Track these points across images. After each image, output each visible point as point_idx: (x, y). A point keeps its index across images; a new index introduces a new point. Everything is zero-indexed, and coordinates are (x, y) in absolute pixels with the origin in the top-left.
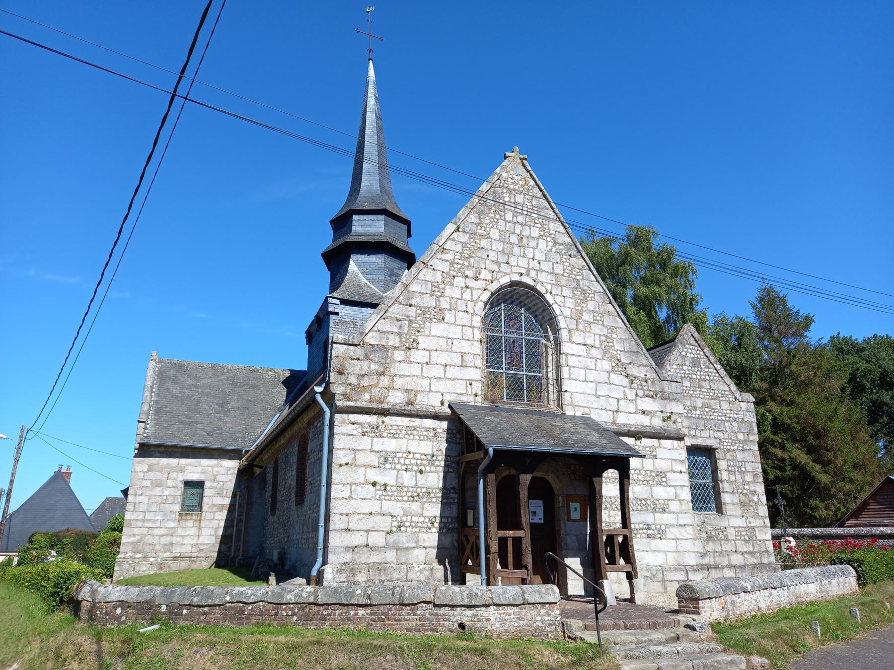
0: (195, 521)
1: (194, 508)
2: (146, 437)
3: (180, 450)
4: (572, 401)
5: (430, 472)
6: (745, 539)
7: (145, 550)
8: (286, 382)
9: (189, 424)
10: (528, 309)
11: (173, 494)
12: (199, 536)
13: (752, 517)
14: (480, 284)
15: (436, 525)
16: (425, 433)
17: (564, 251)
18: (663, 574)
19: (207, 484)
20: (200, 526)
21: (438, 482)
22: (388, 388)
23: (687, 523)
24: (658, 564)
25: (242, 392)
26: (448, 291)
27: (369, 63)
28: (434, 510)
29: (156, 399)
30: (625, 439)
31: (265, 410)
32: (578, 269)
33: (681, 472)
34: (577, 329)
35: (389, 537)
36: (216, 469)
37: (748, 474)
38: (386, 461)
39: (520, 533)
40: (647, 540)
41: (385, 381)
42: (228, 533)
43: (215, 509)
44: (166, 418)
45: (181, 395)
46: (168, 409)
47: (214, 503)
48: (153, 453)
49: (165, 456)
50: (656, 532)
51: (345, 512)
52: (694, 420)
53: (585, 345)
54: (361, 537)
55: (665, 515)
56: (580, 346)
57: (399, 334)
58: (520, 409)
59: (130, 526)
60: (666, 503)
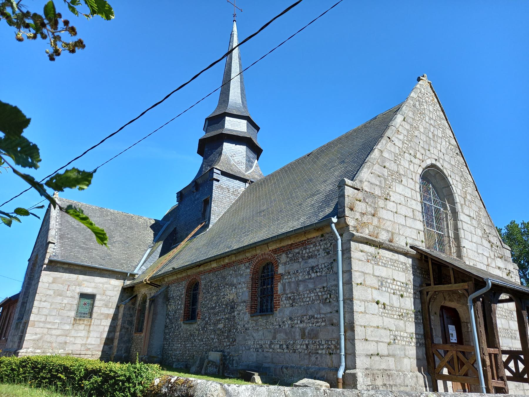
0: (86, 325)
1: (85, 315)
2: (54, 256)
3: (80, 268)
4: (467, 255)
7: (44, 347)
8: (152, 227)
9: (87, 249)
11: (70, 303)
12: (88, 337)
15: (414, 340)
16: (401, 266)
19: (98, 297)
20: (89, 330)
25: (122, 231)
27: (233, 25)
29: (59, 227)
31: (140, 245)
34: (465, 204)
35: (390, 347)
36: (106, 286)
38: (382, 284)
42: (110, 337)
43: (102, 317)
44: (69, 243)
45: (78, 227)
46: (69, 236)
47: (101, 312)
48: (59, 269)
49: (68, 272)
51: (363, 324)
53: (470, 216)
54: (374, 346)
59: (33, 326)
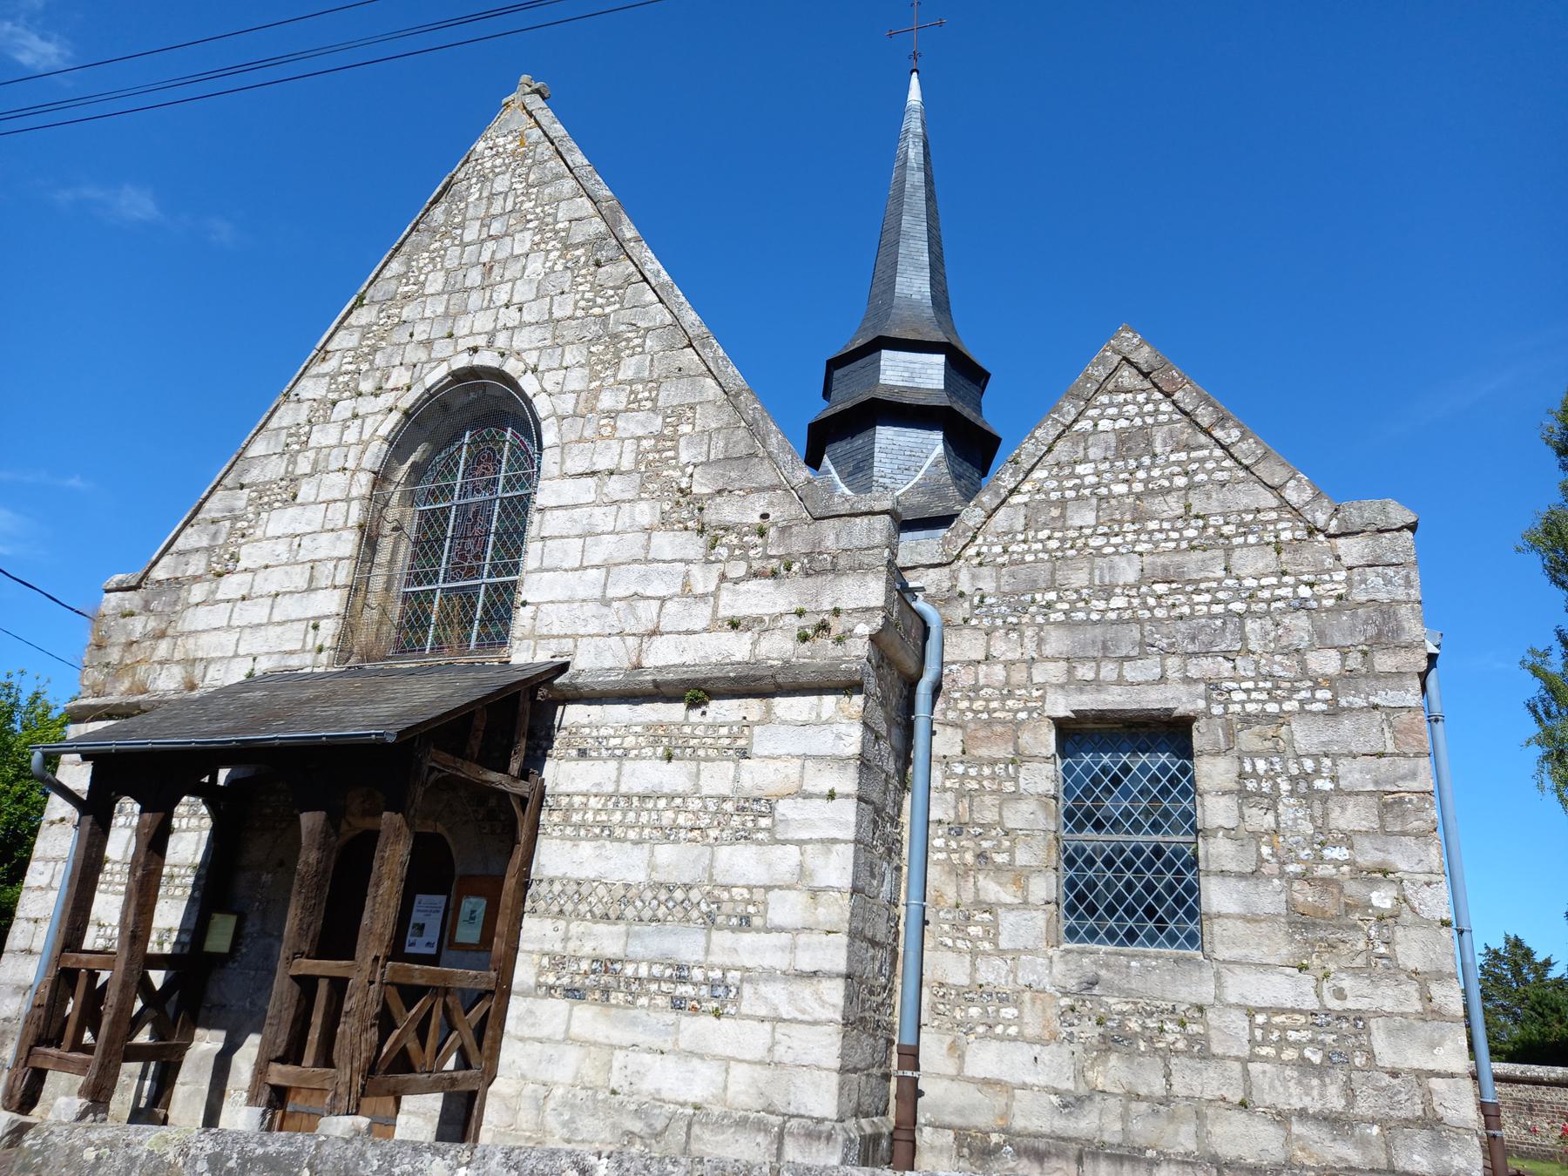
5: (188, 829)
6: (1303, 1058)
13: (1355, 972)
17: (583, 259)
18: (688, 1134)
21: (196, 853)
23: (826, 967)
24: (691, 1099)
32: (612, 288)
33: (832, 796)
37: (1351, 801)
40: (671, 1017)
50: (704, 991)
52: (1098, 630)
53: (594, 473)
55: (747, 938)
56: (583, 480)
58: (407, 666)
60: (758, 895)
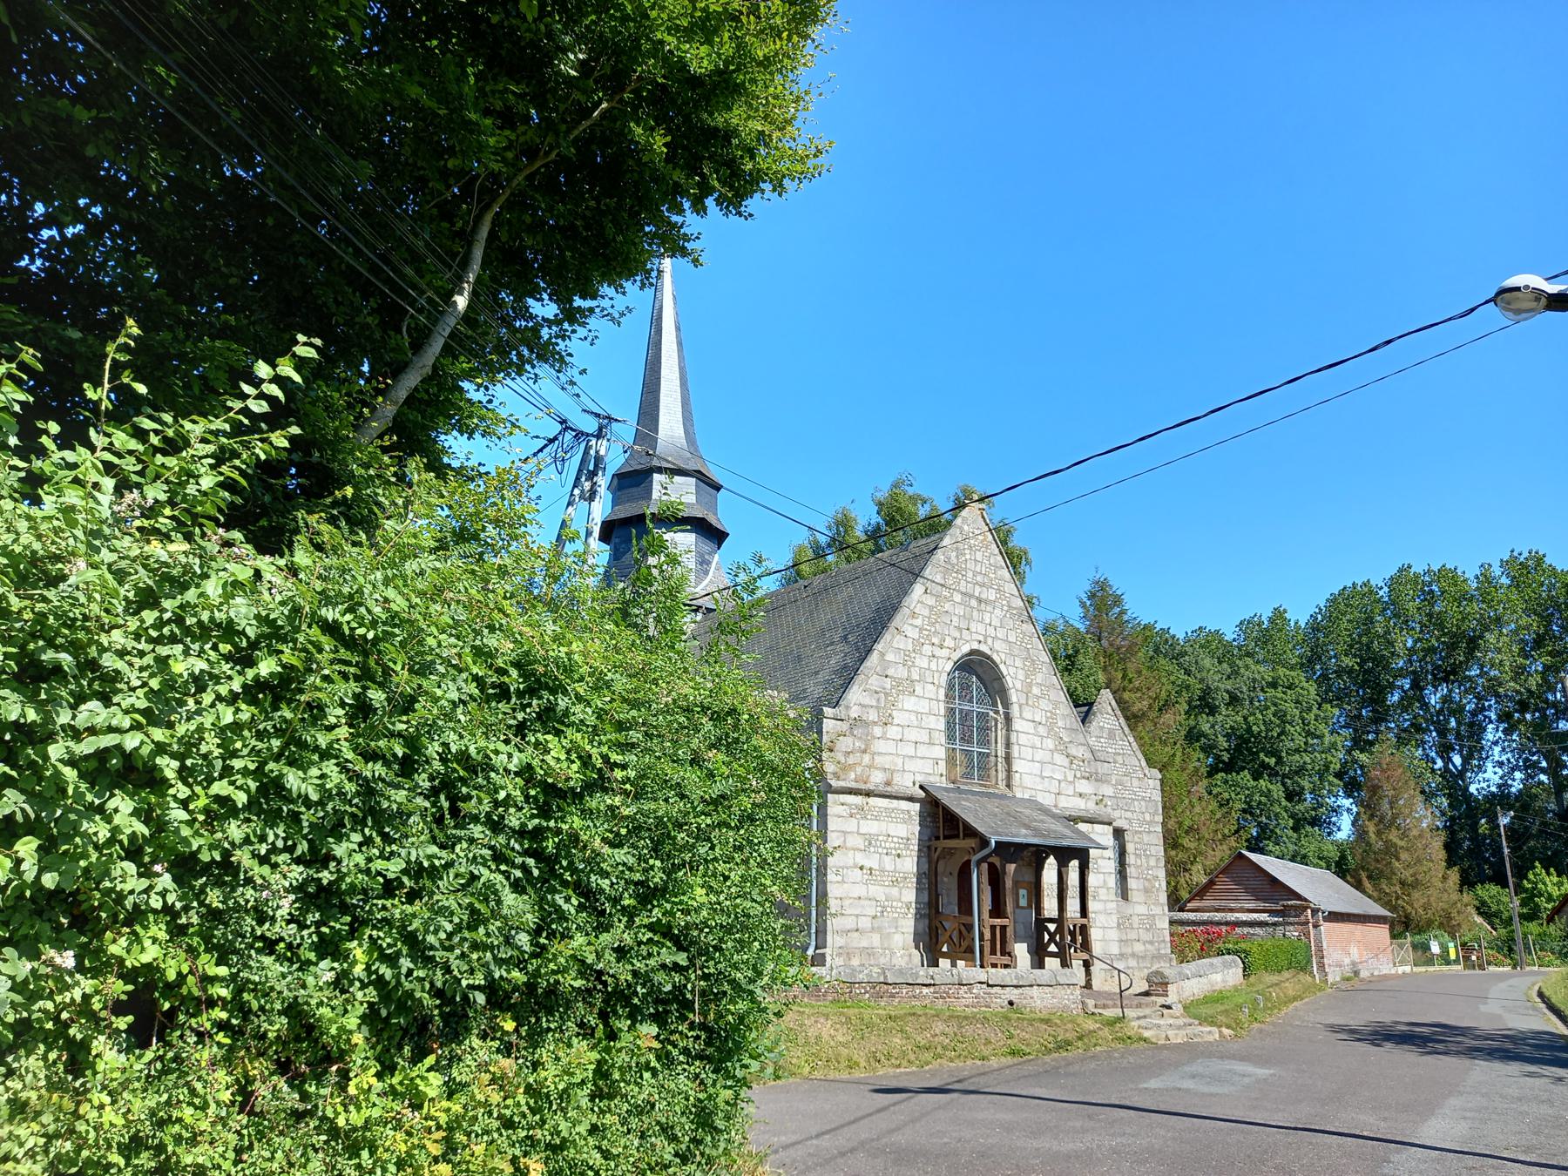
10: (978, 677)
14: (945, 653)
22: (870, 767)
26: (918, 662)
28: (910, 895)
30: (1082, 827)
38: (870, 844)
39: (1004, 922)
41: (867, 758)
57: (878, 708)
